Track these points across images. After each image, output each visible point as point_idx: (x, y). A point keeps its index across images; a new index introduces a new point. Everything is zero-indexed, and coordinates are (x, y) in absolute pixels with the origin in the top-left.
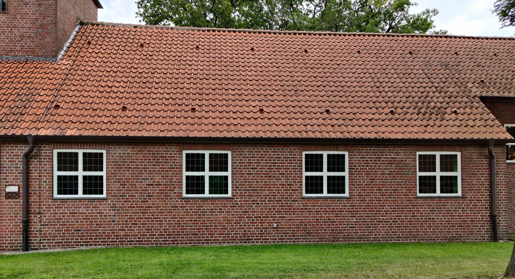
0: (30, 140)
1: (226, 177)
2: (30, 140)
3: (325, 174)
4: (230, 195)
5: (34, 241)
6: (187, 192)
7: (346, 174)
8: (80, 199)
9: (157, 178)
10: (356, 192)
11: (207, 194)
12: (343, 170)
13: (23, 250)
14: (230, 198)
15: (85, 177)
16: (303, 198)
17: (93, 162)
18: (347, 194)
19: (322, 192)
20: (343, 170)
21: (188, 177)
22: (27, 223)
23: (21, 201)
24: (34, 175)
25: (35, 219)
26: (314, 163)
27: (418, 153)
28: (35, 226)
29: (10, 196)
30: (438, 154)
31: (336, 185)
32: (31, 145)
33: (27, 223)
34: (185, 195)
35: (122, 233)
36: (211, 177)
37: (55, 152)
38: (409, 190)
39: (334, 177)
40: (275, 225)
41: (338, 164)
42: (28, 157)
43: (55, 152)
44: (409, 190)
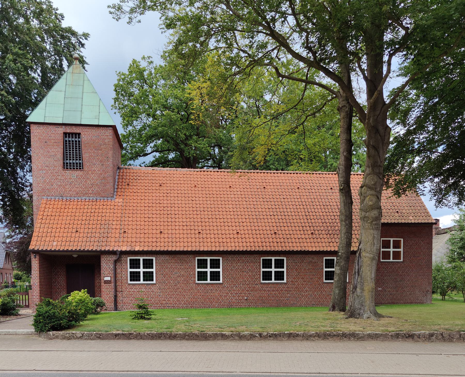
0: (118, 253)
1: (219, 272)
2: (118, 253)
3: (273, 270)
4: (154, 282)
5: (119, 306)
6: (198, 280)
7: (285, 270)
8: (142, 284)
9: (182, 273)
10: (290, 280)
11: (209, 281)
12: (283, 268)
13: (114, 310)
14: (285, 283)
15: (144, 272)
16: (261, 283)
17: (148, 264)
18: (285, 281)
19: (207, 280)
20: (283, 268)
21: (198, 272)
22: (116, 296)
23: (113, 285)
24: (119, 271)
25: (119, 294)
26: (267, 264)
27: (325, 258)
28: (120, 299)
29: (106, 282)
30: (273, 259)
31: (279, 276)
32: (118, 255)
33: (116, 296)
34: (197, 282)
35: (164, 302)
36: (211, 272)
37: (129, 258)
38: (319, 278)
39: (214, 272)
40: (246, 298)
41: (136, 264)
42: (116, 262)
43: (129, 258)
44: (319, 278)
